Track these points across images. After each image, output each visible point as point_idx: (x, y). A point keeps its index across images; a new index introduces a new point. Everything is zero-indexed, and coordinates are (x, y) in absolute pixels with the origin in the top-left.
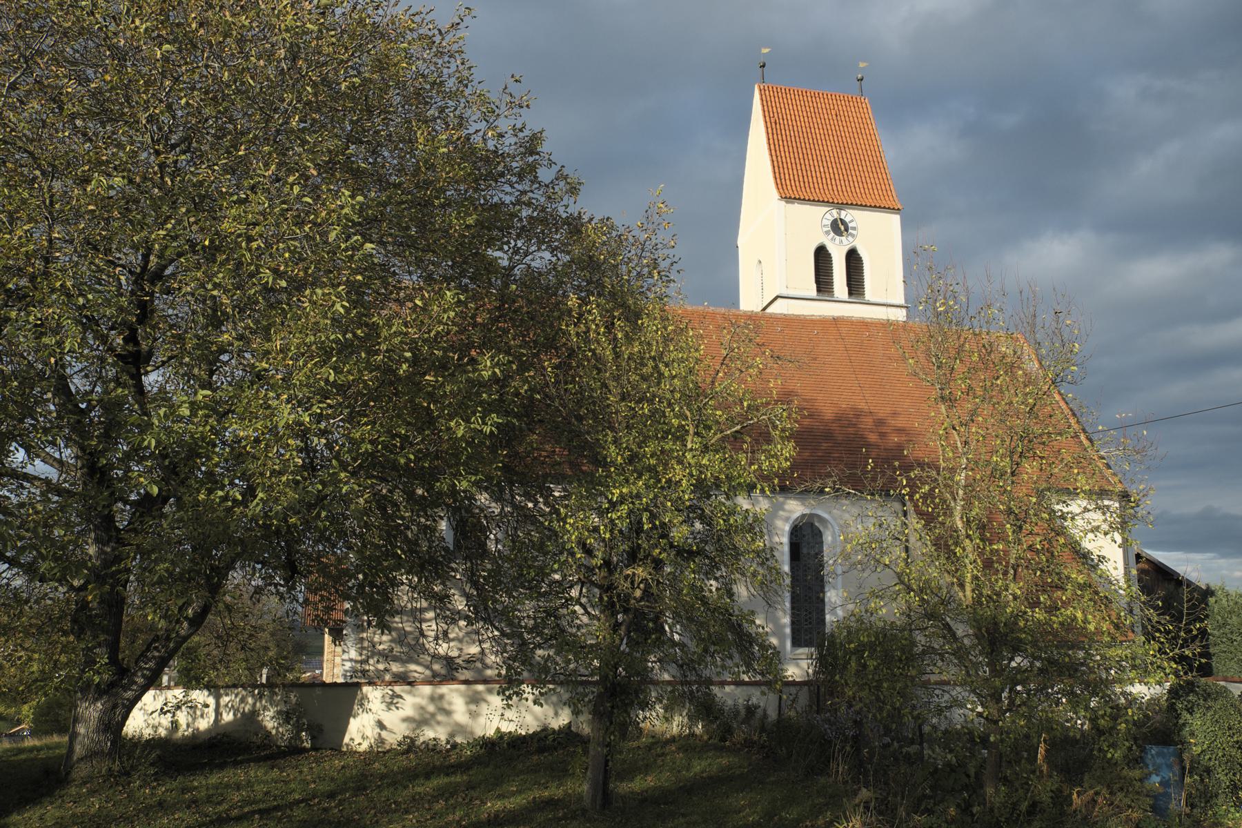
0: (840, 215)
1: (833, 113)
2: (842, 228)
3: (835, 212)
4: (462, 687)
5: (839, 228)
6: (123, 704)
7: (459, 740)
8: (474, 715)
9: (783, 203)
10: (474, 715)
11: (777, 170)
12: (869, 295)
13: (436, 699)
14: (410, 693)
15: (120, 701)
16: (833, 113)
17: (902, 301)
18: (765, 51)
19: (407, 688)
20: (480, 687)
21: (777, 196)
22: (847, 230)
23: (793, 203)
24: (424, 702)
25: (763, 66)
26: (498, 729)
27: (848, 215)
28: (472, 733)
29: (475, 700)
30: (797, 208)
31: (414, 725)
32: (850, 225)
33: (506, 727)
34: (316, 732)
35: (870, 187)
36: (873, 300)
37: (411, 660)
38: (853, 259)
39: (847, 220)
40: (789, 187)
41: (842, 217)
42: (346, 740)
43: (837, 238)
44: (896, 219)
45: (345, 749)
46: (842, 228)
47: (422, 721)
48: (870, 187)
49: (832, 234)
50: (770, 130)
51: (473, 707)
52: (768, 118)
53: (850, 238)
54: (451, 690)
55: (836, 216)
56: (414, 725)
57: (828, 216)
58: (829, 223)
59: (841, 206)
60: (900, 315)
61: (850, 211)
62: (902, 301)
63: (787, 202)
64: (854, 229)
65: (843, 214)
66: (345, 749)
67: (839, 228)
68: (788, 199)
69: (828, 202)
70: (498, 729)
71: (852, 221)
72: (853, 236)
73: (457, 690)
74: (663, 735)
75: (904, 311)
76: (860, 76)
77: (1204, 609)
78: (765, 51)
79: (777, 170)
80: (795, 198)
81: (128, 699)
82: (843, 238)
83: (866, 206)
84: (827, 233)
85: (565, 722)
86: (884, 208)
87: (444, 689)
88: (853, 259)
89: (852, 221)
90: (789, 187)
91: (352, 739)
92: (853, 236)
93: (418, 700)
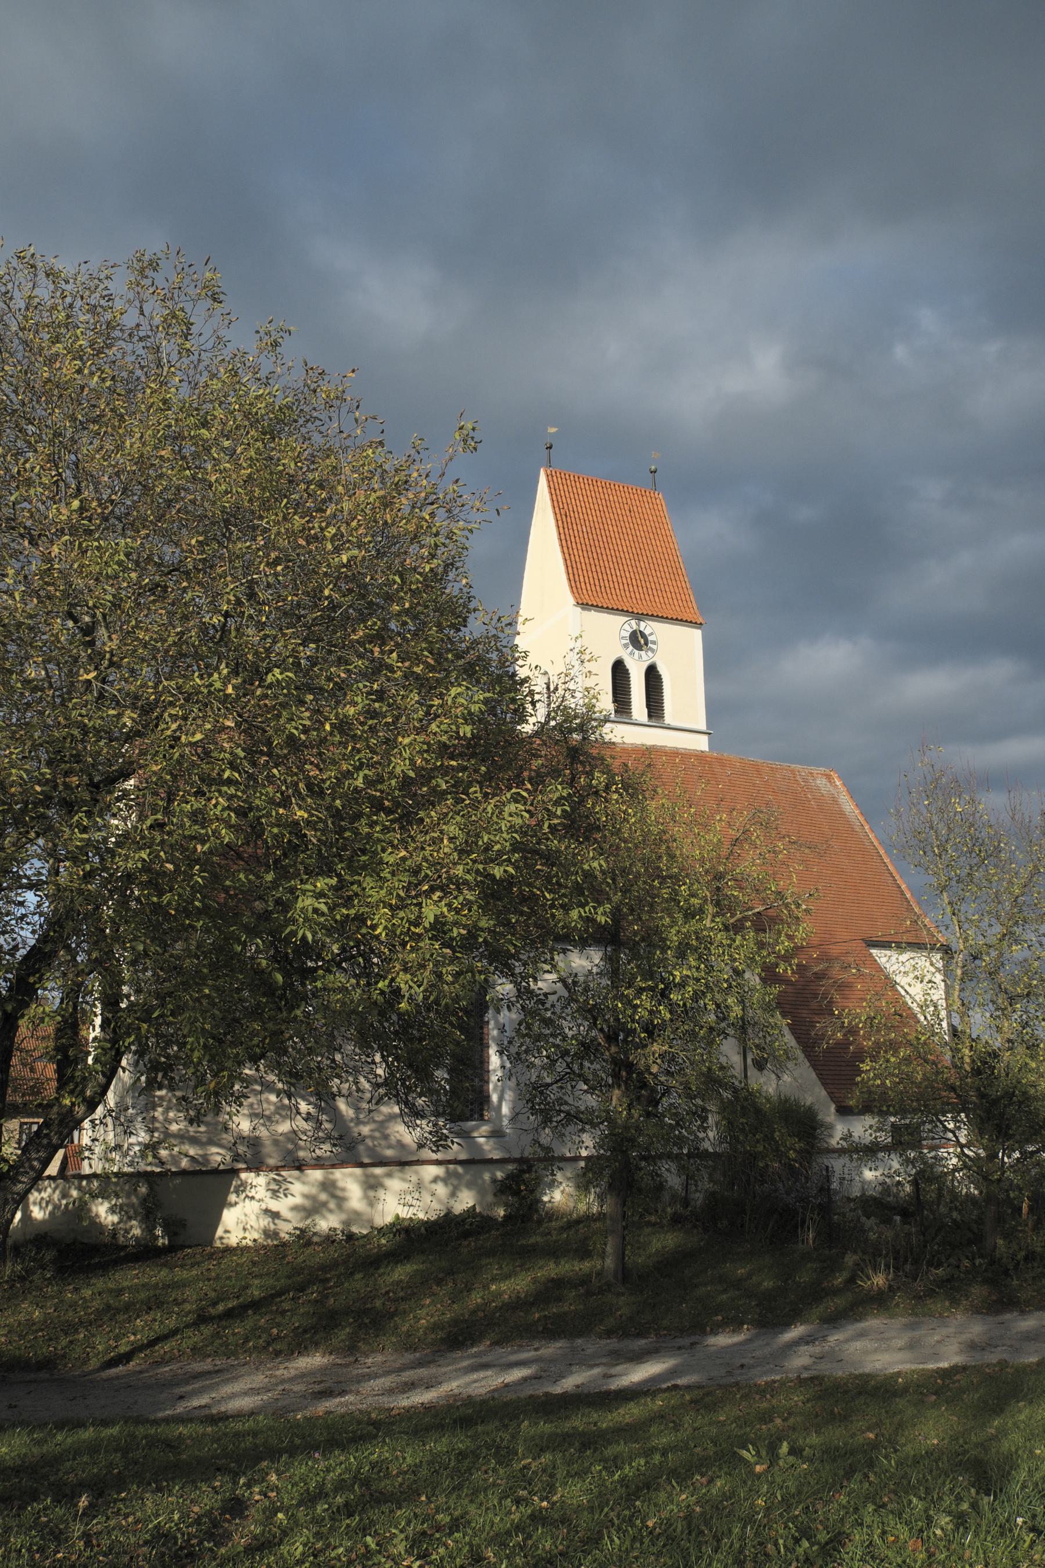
0: (638, 625)
1: (627, 507)
2: (642, 642)
3: (633, 622)
4: (358, 1171)
5: (638, 640)
6: (13, 1199)
7: (355, 1229)
8: (372, 1203)
9: (579, 609)
10: (372, 1203)
11: (570, 571)
12: (669, 718)
13: (328, 1186)
14: (298, 1179)
15: (9, 1196)
16: (627, 507)
17: (703, 727)
18: (552, 430)
19: (296, 1173)
20: (378, 1171)
21: (571, 601)
22: (646, 644)
23: (590, 610)
24: (314, 1191)
25: (550, 448)
26: (397, 1217)
27: (648, 627)
28: (370, 1221)
29: (372, 1186)
30: (593, 615)
31: (303, 1214)
32: (650, 638)
33: (405, 1213)
34: (173, 1227)
35: (605, 558)
36: (673, 724)
37: (211, 1142)
38: (652, 676)
39: (647, 632)
40: (585, 591)
41: (642, 629)
42: (220, 1232)
43: (636, 652)
44: (697, 634)
45: (218, 1244)
46: (642, 642)
47: (312, 1208)
48: (605, 558)
49: (631, 648)
50: (560, 523)
51: (371, 1194)
52: (557, 509)
53: (650, 653)
54: (344, 1175)
55: (635, 627)
56: (303, 1214)
57: (626, 627)
58: (628, 635)
59: (640, 617)
60: (701, 744)
61: (650, 623)
62: (703, 727)
63: (583, 609)
64: (654, 643)
65: (643, 624)
66: (218, 1244)
67: (638, 640)
68: (584, 605)
69: (627, 611)
70: (397, 1217)
71: (651, 634)
72: (653, 651)
73: (351, 1175)
74: (571, 1215)
75: (705, 738)
76: (653, 468)
77: (409, 1016)
78: (552, 430)
79: (570, 571)
80: (592, 605)
81: (18, 1194)
82: (643, 653)
83: (667, 618)
84: (626, 646)
85: (469, 1206)
86: (686, 621)
87: (338, 1174)
88: (652, 676)
89: (651, 634)
90: (585, 591)
91: (227, 1231)
92: (653, 651)
93: (306, 1189)
